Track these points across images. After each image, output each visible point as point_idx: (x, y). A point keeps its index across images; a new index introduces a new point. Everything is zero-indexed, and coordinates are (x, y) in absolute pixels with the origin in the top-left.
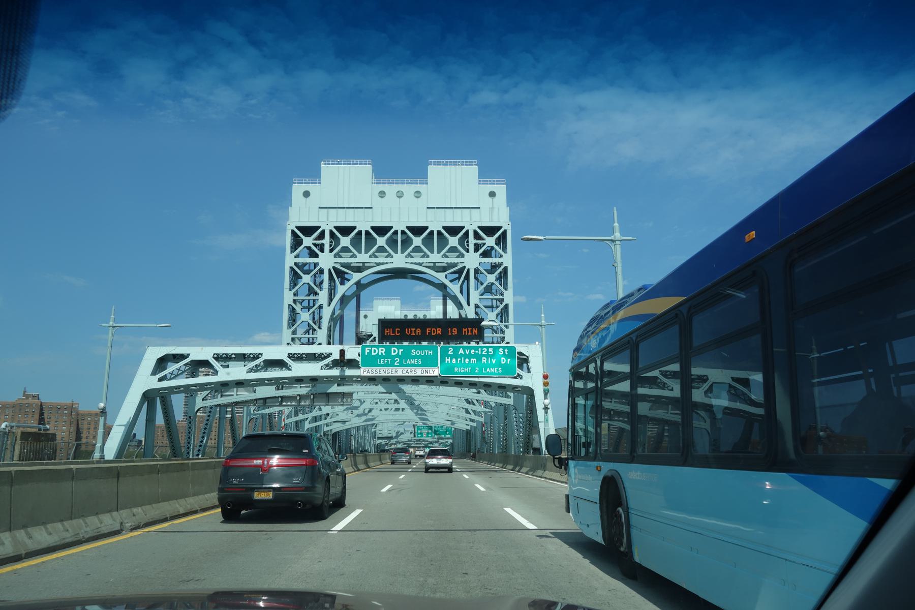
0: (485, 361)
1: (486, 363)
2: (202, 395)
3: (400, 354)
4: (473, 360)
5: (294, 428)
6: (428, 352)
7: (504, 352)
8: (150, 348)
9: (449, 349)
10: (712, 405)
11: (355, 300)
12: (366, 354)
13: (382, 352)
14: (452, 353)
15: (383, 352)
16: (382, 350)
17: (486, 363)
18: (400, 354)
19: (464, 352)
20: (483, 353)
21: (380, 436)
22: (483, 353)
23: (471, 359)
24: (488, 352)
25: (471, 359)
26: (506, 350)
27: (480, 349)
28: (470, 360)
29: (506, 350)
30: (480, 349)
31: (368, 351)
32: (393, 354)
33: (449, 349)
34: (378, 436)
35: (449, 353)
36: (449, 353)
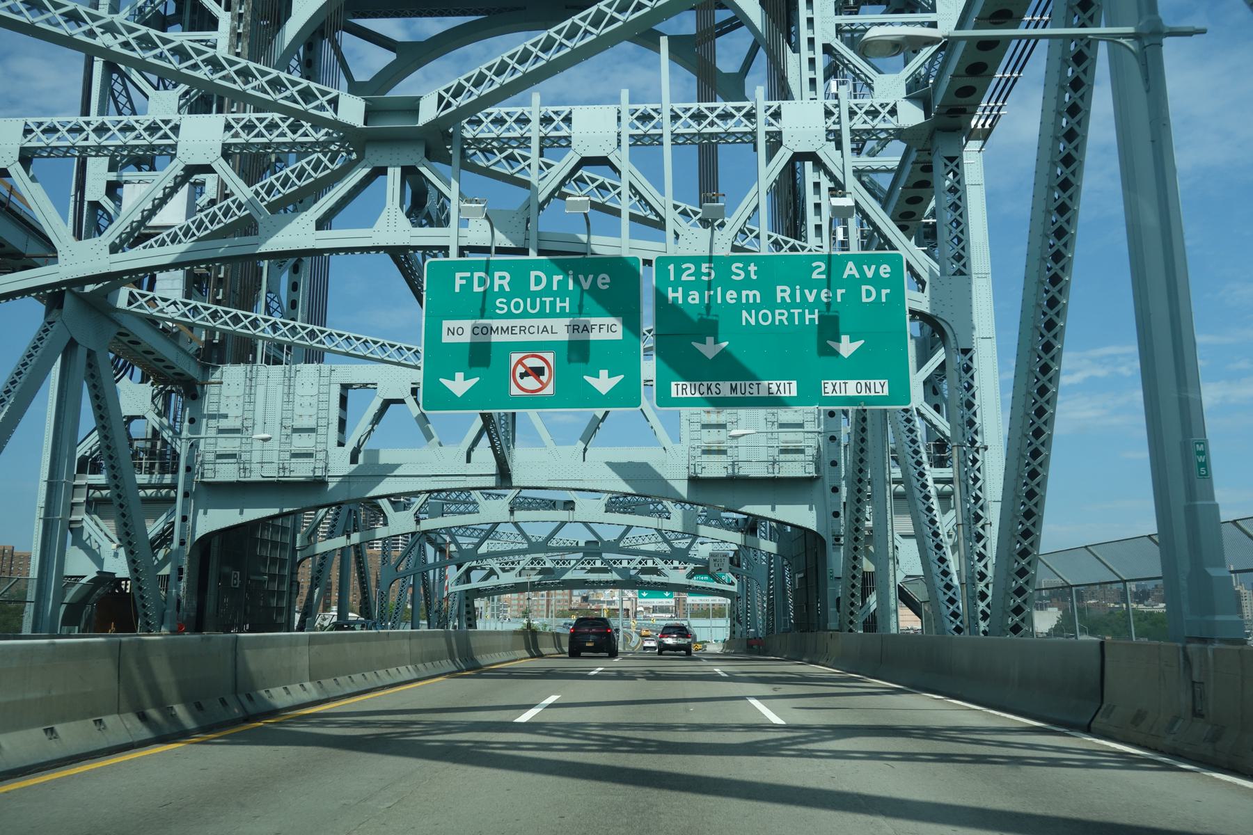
0: (786, 295)
1: (788, 300)
2: (98, 540)
3: (555, 288)
4: (751, 293)
5: (434, 586)
6: (802, 316)
7: (747, 273)
8: (44, 307)
9: (814, 265)
10: (839, 353)
11: (876, 60)
12: (457, 290)
13: (502, 282)
14: (693, 278)
15: (505, 283)
16: (502, 278)
17: (788, 300)
18: (555, 288)
19: (861, 272)
20: (684, 278)
21: (227, 473)
22: (684, 278)
23: (744, 293)
24: (698, 273)
25: (744, 293)
26: (752, 268)
27: (671, 267)
28: (739, 295)
29: (752, 268)
30: (671, 267)
31: (464, 282)
32: (533, 288)
33: (814, 265)
34: (209, 477)
35: (815, 276)
36: (815, 276)
